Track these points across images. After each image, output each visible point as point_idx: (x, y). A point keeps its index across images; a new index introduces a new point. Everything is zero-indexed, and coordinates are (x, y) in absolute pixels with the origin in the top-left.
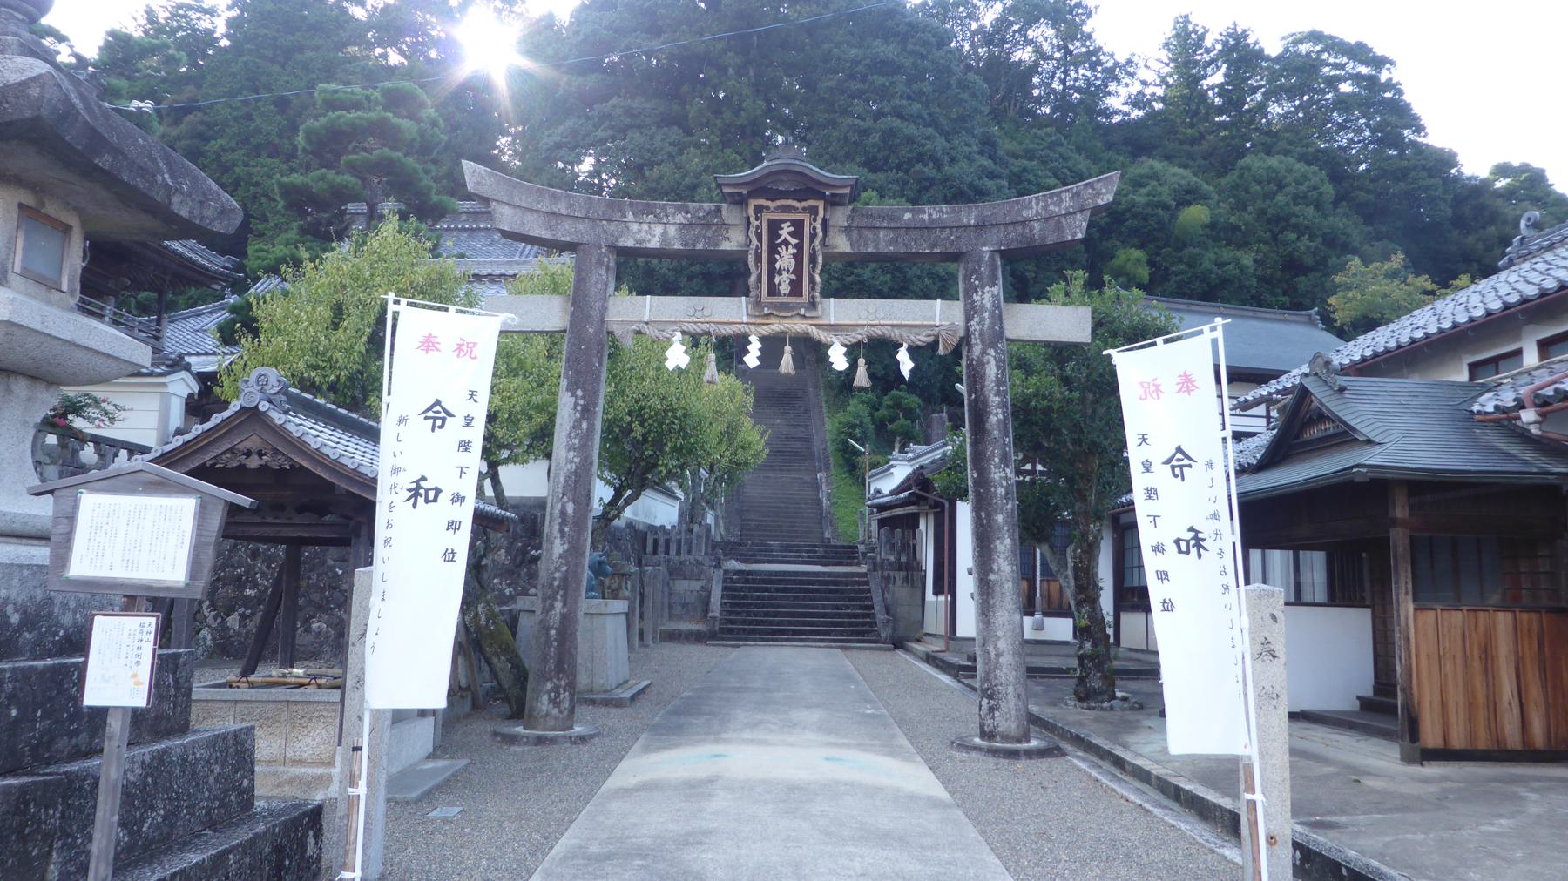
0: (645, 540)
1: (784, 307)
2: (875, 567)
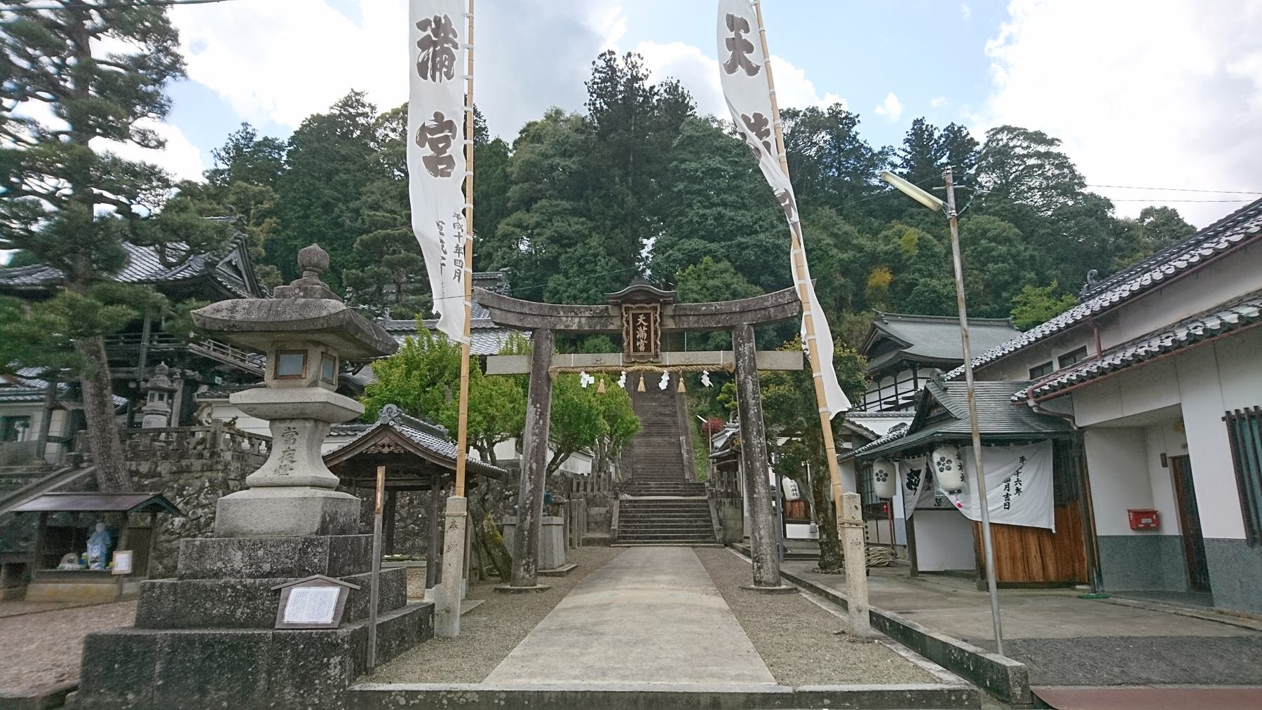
0: (571, 483)
1: (642, 357)
2: (713, 496)
